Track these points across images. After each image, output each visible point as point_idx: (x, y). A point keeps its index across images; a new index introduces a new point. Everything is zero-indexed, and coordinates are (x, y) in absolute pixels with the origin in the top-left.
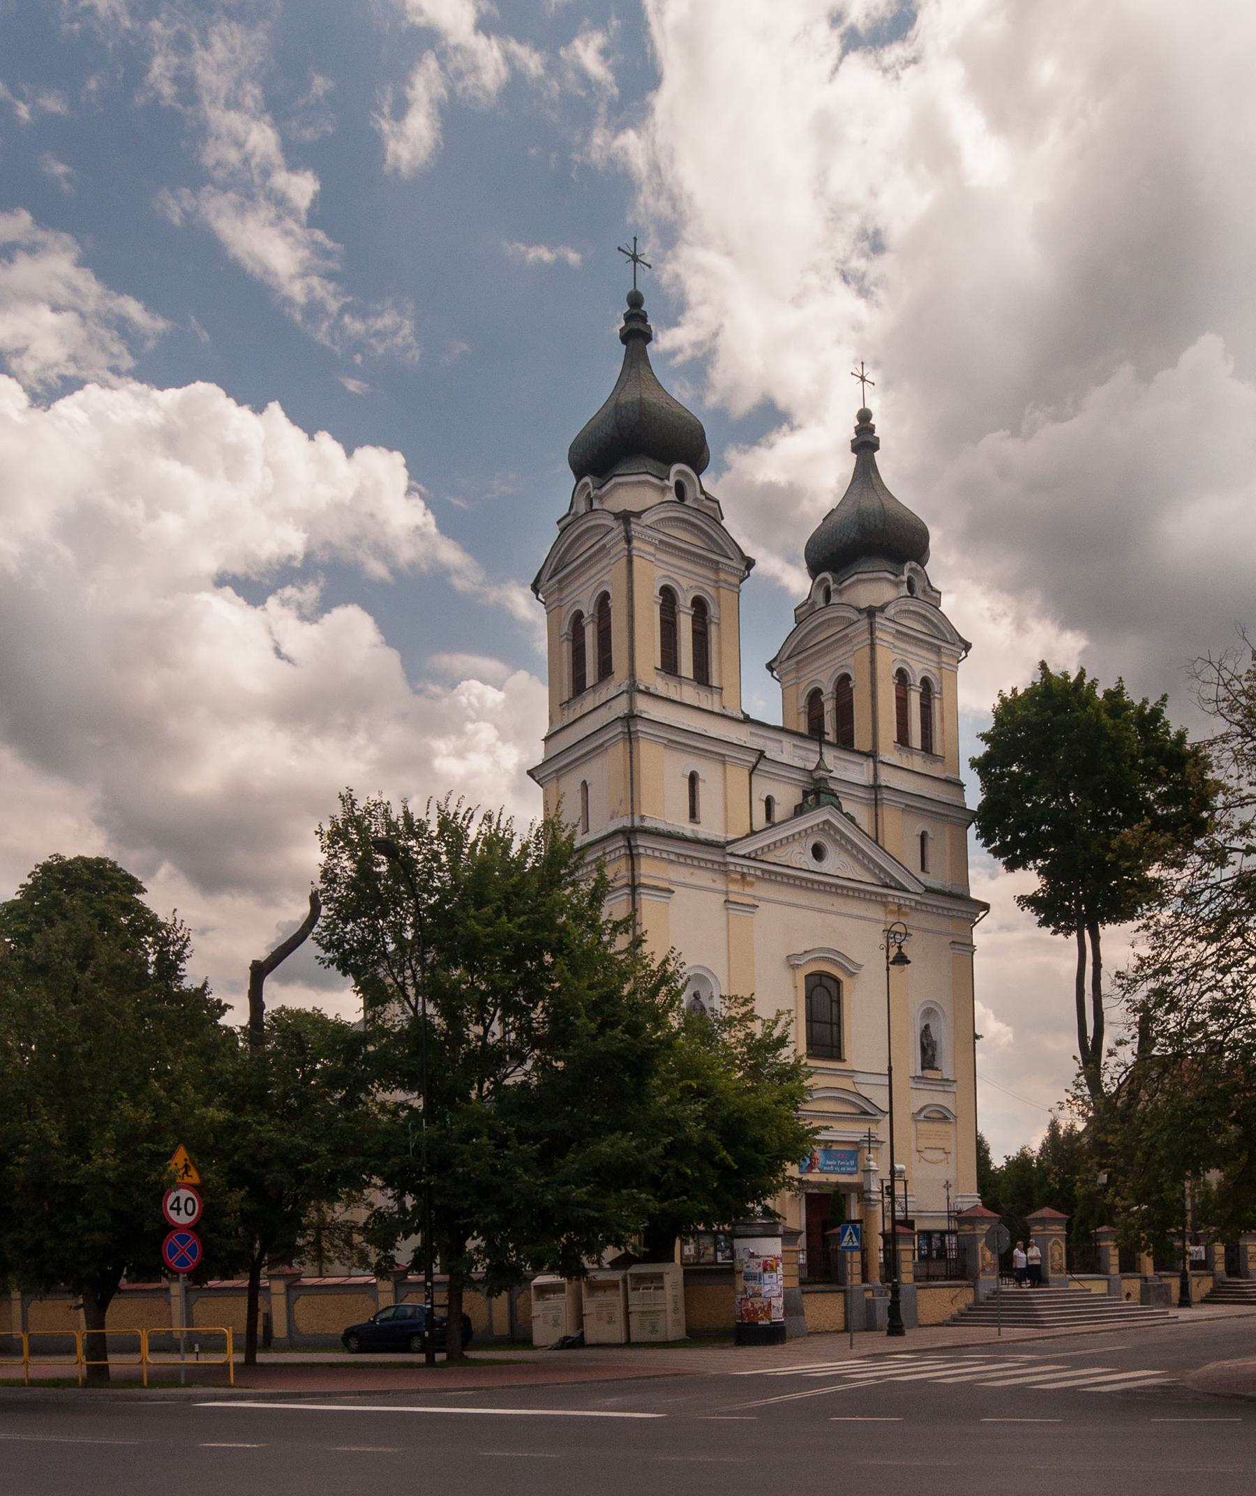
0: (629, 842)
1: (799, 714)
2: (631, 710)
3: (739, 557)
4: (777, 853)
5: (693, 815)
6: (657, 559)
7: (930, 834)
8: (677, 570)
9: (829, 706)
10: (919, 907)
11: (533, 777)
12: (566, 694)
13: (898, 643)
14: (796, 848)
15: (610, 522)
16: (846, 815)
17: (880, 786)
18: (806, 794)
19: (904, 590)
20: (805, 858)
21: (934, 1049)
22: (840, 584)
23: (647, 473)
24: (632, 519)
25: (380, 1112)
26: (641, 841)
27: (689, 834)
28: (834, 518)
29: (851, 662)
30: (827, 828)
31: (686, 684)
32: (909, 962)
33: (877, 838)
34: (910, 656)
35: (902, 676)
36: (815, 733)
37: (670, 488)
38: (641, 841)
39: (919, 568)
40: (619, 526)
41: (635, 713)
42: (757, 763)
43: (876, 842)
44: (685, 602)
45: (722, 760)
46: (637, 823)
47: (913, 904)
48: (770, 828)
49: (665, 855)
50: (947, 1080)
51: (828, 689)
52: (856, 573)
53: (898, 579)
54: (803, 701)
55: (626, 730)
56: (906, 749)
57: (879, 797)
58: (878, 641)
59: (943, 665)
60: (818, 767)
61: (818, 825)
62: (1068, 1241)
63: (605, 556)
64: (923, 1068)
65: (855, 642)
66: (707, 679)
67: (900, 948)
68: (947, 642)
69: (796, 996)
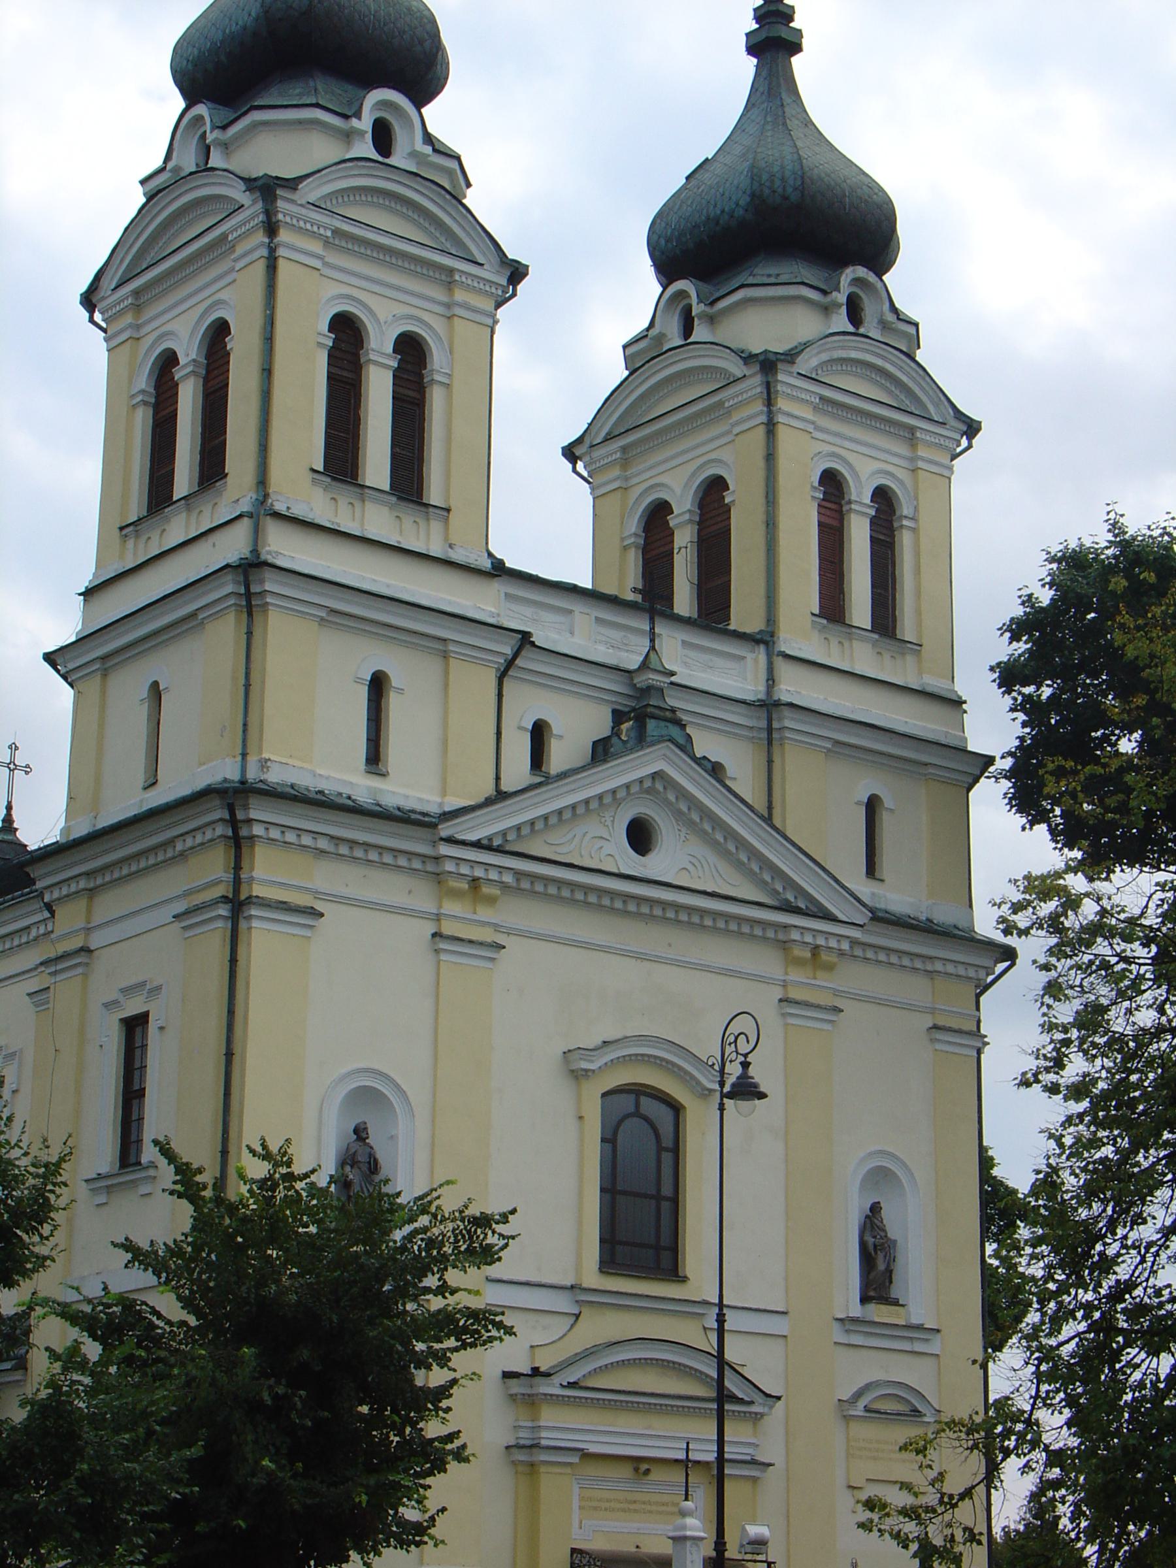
0: (232, 813)
1: (625, 548)
2: (255, 551)
3: (495, 259)
4: (554, 837)
5: (374, 758)
6: (326, 264)
7: (888, 802)
8: (364, 284)
9: (684, 539)
10: (857, 951)
11: (54, 665)
12: (135, 507)
13: (825, 422)
14: (591, 827)
15: (238, 193)
16: (701, 761)
17: (778, 704)
18: (618, 717)
19: (841, 321)
20: (608, 848)
21: (891, 1260)
22: (712, 303)
23: (317, 106)
24: (279, 192)
25: (1081, 791)
26: (258, 811)
27: (363, 798)
28: (718, 168)
29: (725, 454)
31: (375, 501)
32: (762, 1096)
33: (770, 808)
34: (847, 444)
35: (832, 483)
37: (362, 133)
38: (258, 811)
39: (871, 277)
40: (254, 202)
41: (263, 557)
42: (516, 656)
43: (768, 819)
44: (860, 494)
45: (442, 649)
46: (252, 775)
47: (845, 946)
48: (540, 785)
49: (307, 840)
50: (920, 1328)
51: (683, 505)
52: (742, 286)
53: (828, 299)
54: (633, 525)
55: (242, 591)
56: (838, 628)
57: (775, 725)
58: (781, 418)
59: (920, 464)
60: (645, 665)
61: (641, 781)
63: (223, 255)
64: (864, 1300)
65: (736, 417)
66: (420, 495)
67: (745, 1065)
68: (931, 420)
69: (581, 1140)
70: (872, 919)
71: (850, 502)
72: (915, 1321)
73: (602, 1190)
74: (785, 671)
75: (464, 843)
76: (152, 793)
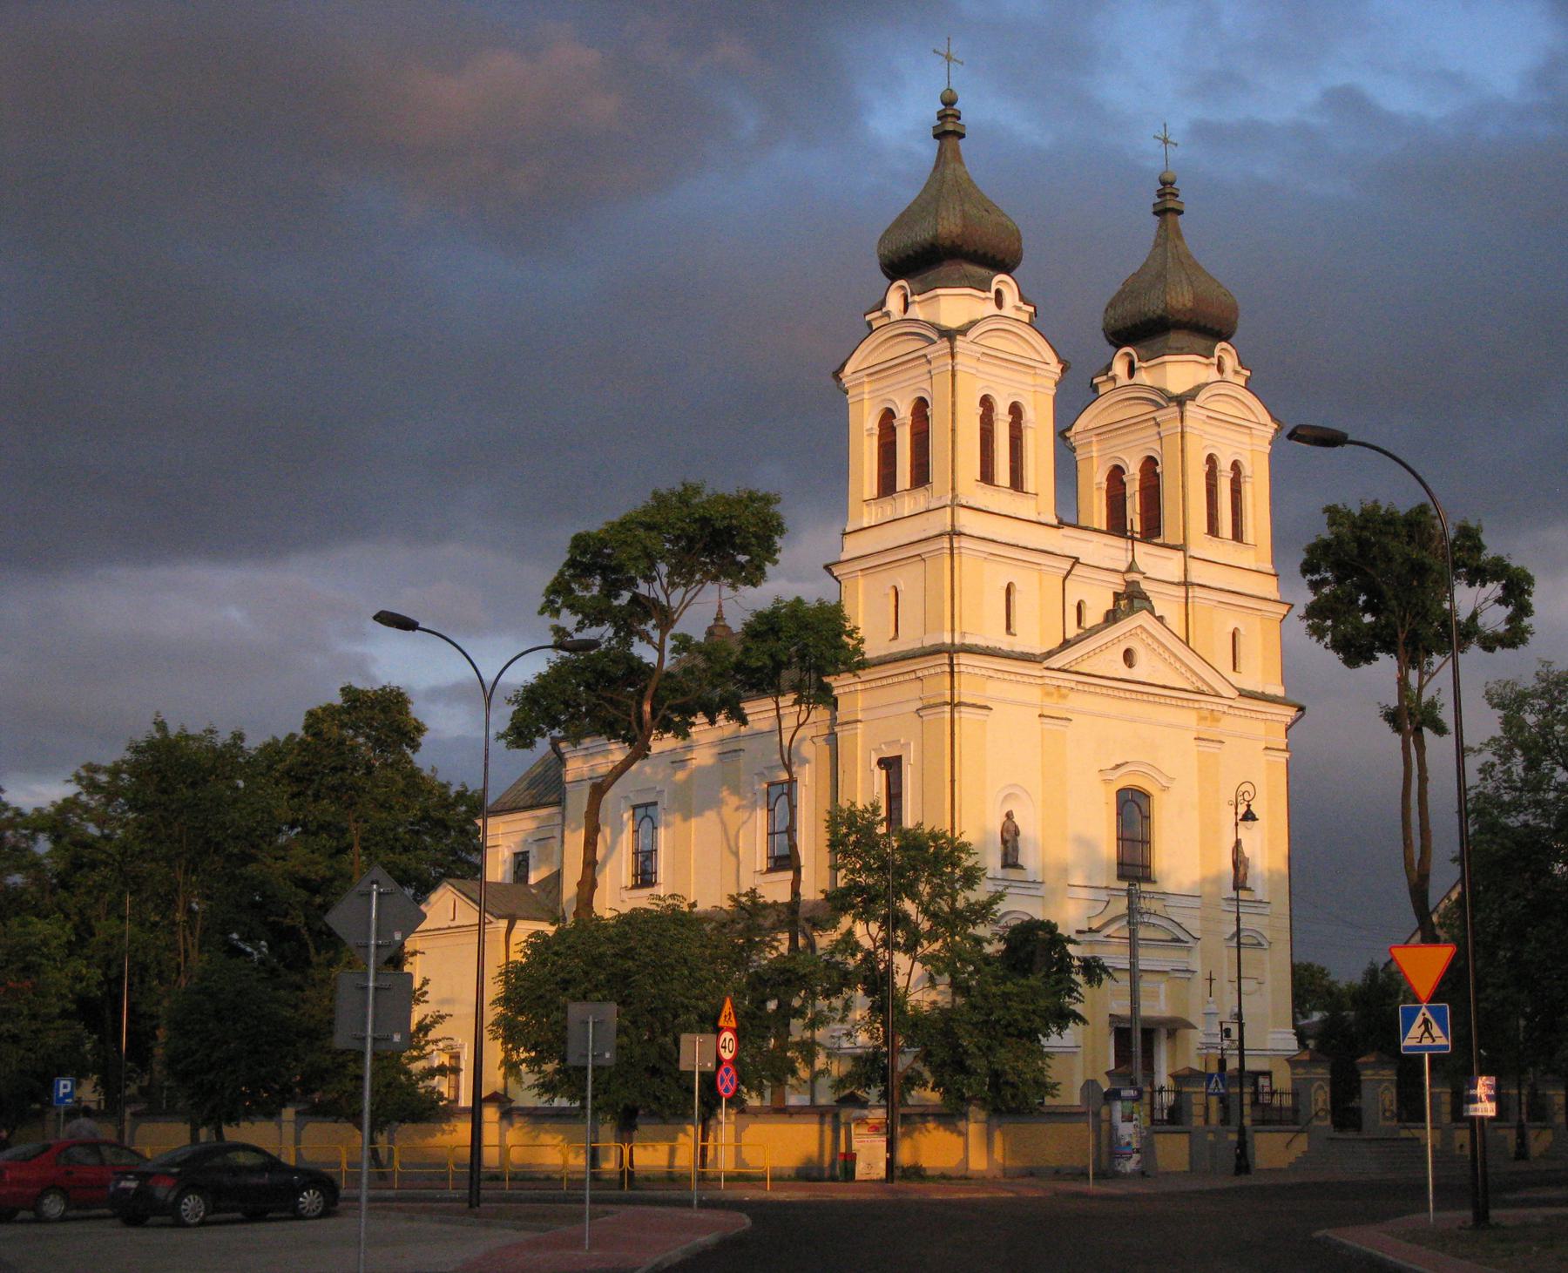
14: (1107, 655)
26: (963, 659)
27: (1006, 647)
30: (1139, 632)
36: (1117, 525)
43: (1187, 643)
44: (1224, 466)
50: (1261, 902)
62: (1399, 1087)
66: (1022, 488)
67: (1249, 806)
70: (1240, 695)
71: (1220, 471)
72: (1258, 898)
73: (1118, 839)
74: (1193, 564)
75: (1053, 669)
76: (895, 643)
